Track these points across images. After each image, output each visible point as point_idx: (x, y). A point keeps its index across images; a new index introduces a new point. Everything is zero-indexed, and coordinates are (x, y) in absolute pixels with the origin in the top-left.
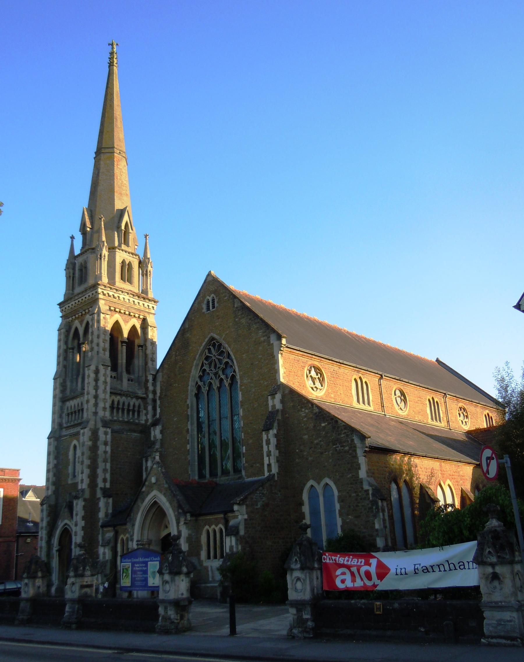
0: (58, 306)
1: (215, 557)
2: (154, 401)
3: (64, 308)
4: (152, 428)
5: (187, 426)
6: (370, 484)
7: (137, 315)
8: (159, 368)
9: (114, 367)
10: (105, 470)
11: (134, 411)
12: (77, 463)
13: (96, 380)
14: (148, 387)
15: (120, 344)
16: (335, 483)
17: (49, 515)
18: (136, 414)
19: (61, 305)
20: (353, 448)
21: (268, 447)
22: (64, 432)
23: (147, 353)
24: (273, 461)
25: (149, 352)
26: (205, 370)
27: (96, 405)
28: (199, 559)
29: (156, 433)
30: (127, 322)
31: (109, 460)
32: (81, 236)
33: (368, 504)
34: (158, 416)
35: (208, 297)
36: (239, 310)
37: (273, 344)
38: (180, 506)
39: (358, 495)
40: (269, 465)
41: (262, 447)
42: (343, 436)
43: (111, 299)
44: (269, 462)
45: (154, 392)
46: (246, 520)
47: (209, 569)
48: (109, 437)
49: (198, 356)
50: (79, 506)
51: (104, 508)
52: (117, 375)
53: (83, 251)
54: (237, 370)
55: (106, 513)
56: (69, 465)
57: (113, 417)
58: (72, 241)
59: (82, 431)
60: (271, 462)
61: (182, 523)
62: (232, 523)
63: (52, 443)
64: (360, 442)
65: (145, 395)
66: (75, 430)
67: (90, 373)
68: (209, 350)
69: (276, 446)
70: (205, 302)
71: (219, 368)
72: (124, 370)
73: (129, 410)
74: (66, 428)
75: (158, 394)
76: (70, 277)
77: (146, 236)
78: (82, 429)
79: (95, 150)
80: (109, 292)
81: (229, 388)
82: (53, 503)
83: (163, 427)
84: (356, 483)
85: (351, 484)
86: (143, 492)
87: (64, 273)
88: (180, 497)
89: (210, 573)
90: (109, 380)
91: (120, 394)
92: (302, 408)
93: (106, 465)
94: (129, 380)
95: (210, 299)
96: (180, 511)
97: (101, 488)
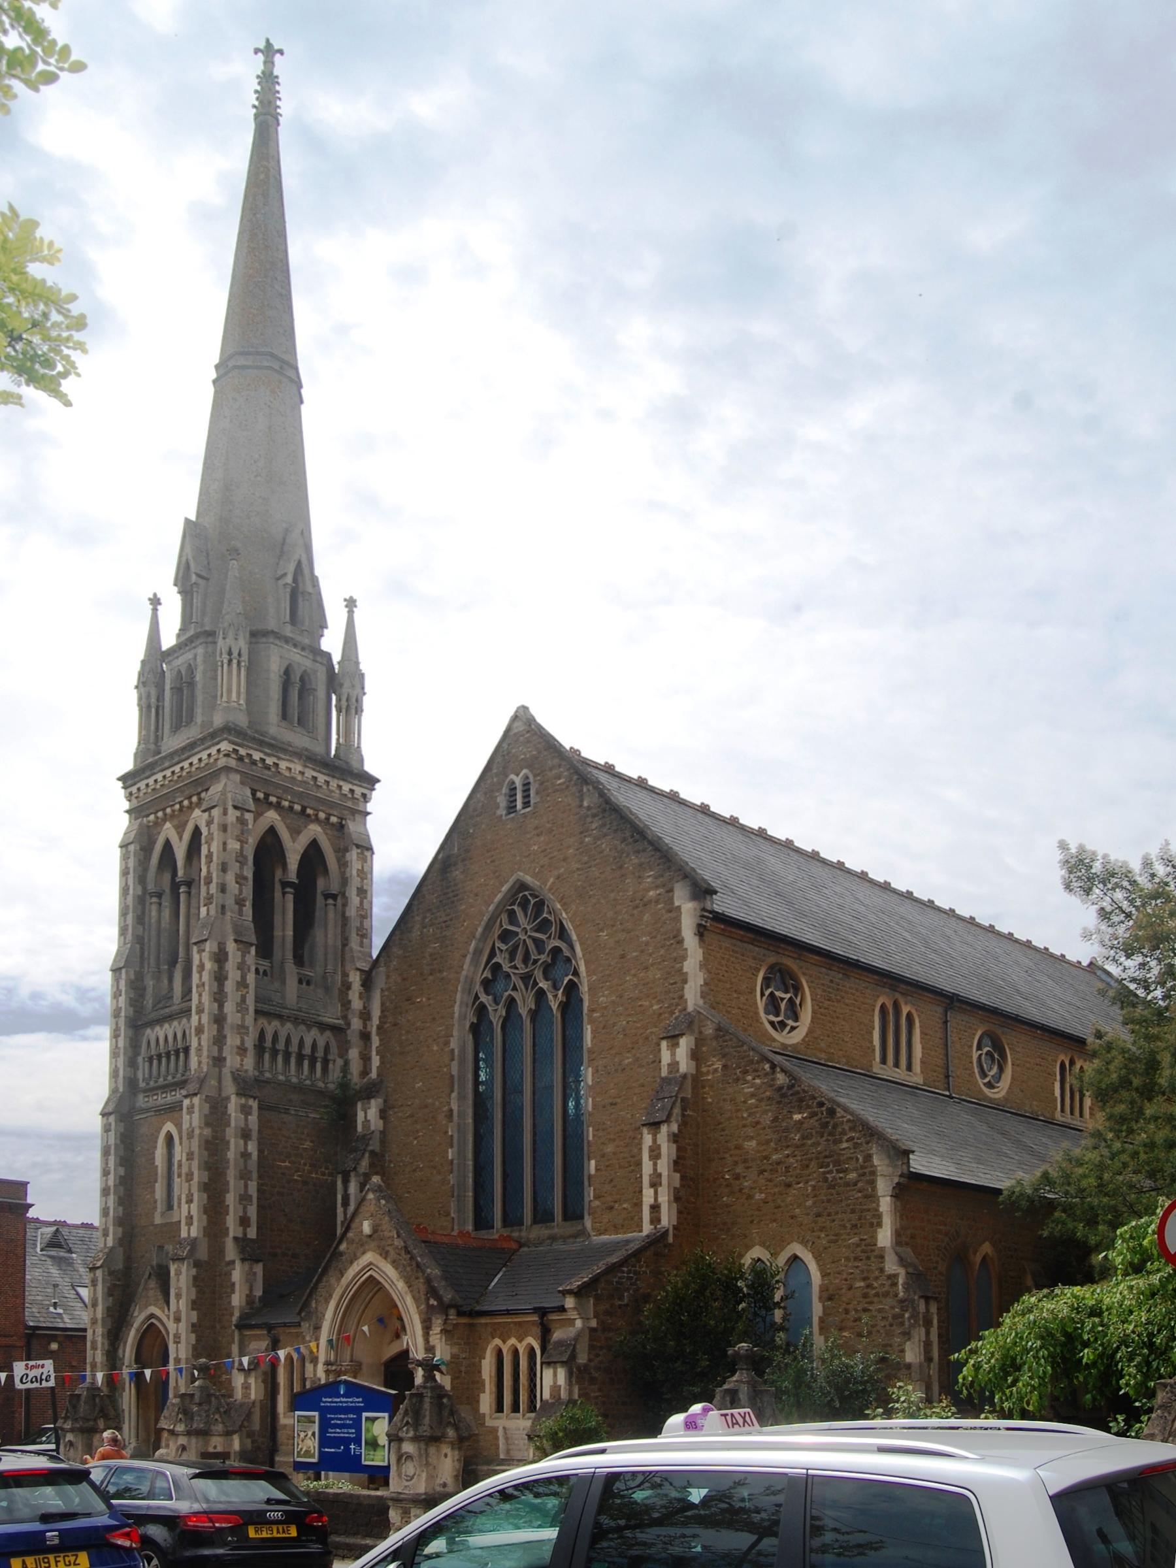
0: (120, 784)
1: (515, 1408)
2: (365, 1036)
3: (134, 789)
4: (359, 1105)
5: (449, 1103)
6: (902, 1261)
7: (322, 815)
8: (378, 957)
9: (265, 949)
10: (244, 1198)
11: (313, 1061)
12: (177, 1180)
13: (220, 978)
14: (349, 1002)
15: (278, 887)
16: (818, 1257)
17: (110, 1292)
18: (319, 1066)
19: (127, 780)
20: (868, 1175)
21: (655, 1165)
22: (141, 1101)
23: (347, 914)
24: (664, 1199)
25: (352, 912)
26: (498, 966)
27: (219, 1040)
28: (476, 1410)
29: (368, 1115)
30: (299, 832)
31: (255, 1175)
32: (179, 597)
33: (893, 1308)
34: (374, 1075)
35: (513, 777)
36: (594, 816)
37: (679, 908)
38: (432, 1292)
39: (869, 1286)
40: (655, 1208)
41: (639, 1164)
42: (845, 1145)
43: (257, 771)
44: (656, 1199)
45: (366, 1015)
46: (592, 1330)
47: (500, 1433)
48: (253, 1119)
49: (480, 930)
50: (181, 1278)
51: (242, 1284)
52: (272, 967)
53: (183, 639)
54: (582, 969)
55: (247, 1296)
56: (156, 1181)
57: (261, 1073)
58: (155, 610)
59: (186, 1102)
60: (660, 1200)
61: (436, 1329)
62: (557, 1335)
63: (113, 1127)
64: (887, 1162)
65: (341, 1022)
66: (170, 1098)
67: (203, 959)
68: (512, 915)
69: (676, 1163)
70: (505, 790)
71: (535, 961)
72: (289, 955)
73: (300, 1058)
74: (145, 1091)
75: (376, 1021)
76: (149, 707)
77: (351, 603)
78: (186, 1097)
79: (216, 360)
80: (251, 752)
81: (559, 1016)
82: (119, 1266)
83: (385, 1101)
84: (868, 1258)
85: (856, 1259)
87: (133, 696)
88: (434, 1271)
89: (501, 1441)
90: (251, 978)
91: (280, 1017)
92: (745, 1072)
93: (246, 1186)
94: (300, 982)
95: (518, 781)
96: (433, 1302)
97: (236, 1239)
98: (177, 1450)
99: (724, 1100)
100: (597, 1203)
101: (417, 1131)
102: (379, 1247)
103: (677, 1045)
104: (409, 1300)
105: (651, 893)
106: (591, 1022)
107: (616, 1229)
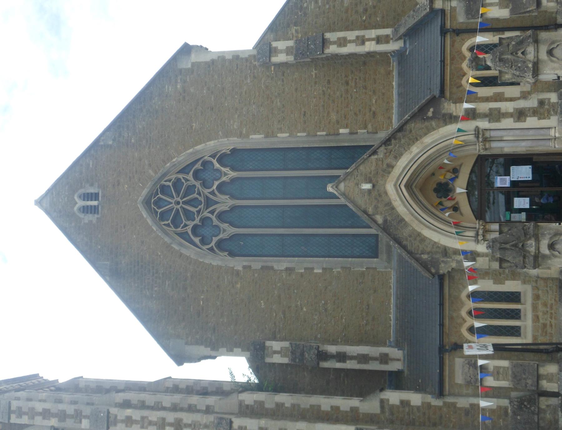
21: (350, 42)
86: (385, 221)
95: (81, 203)
98: (552, 61)
99: (316, 23)
100: (370, 126)
101: (296, 306)
102: (383, 176)
103: (276, 48)
104: (428, 140)
105: (179, 86)
106: (247, 136)
107: (389, 110)
